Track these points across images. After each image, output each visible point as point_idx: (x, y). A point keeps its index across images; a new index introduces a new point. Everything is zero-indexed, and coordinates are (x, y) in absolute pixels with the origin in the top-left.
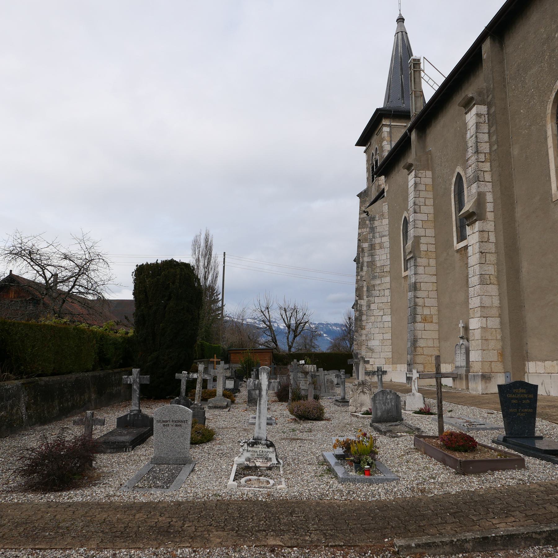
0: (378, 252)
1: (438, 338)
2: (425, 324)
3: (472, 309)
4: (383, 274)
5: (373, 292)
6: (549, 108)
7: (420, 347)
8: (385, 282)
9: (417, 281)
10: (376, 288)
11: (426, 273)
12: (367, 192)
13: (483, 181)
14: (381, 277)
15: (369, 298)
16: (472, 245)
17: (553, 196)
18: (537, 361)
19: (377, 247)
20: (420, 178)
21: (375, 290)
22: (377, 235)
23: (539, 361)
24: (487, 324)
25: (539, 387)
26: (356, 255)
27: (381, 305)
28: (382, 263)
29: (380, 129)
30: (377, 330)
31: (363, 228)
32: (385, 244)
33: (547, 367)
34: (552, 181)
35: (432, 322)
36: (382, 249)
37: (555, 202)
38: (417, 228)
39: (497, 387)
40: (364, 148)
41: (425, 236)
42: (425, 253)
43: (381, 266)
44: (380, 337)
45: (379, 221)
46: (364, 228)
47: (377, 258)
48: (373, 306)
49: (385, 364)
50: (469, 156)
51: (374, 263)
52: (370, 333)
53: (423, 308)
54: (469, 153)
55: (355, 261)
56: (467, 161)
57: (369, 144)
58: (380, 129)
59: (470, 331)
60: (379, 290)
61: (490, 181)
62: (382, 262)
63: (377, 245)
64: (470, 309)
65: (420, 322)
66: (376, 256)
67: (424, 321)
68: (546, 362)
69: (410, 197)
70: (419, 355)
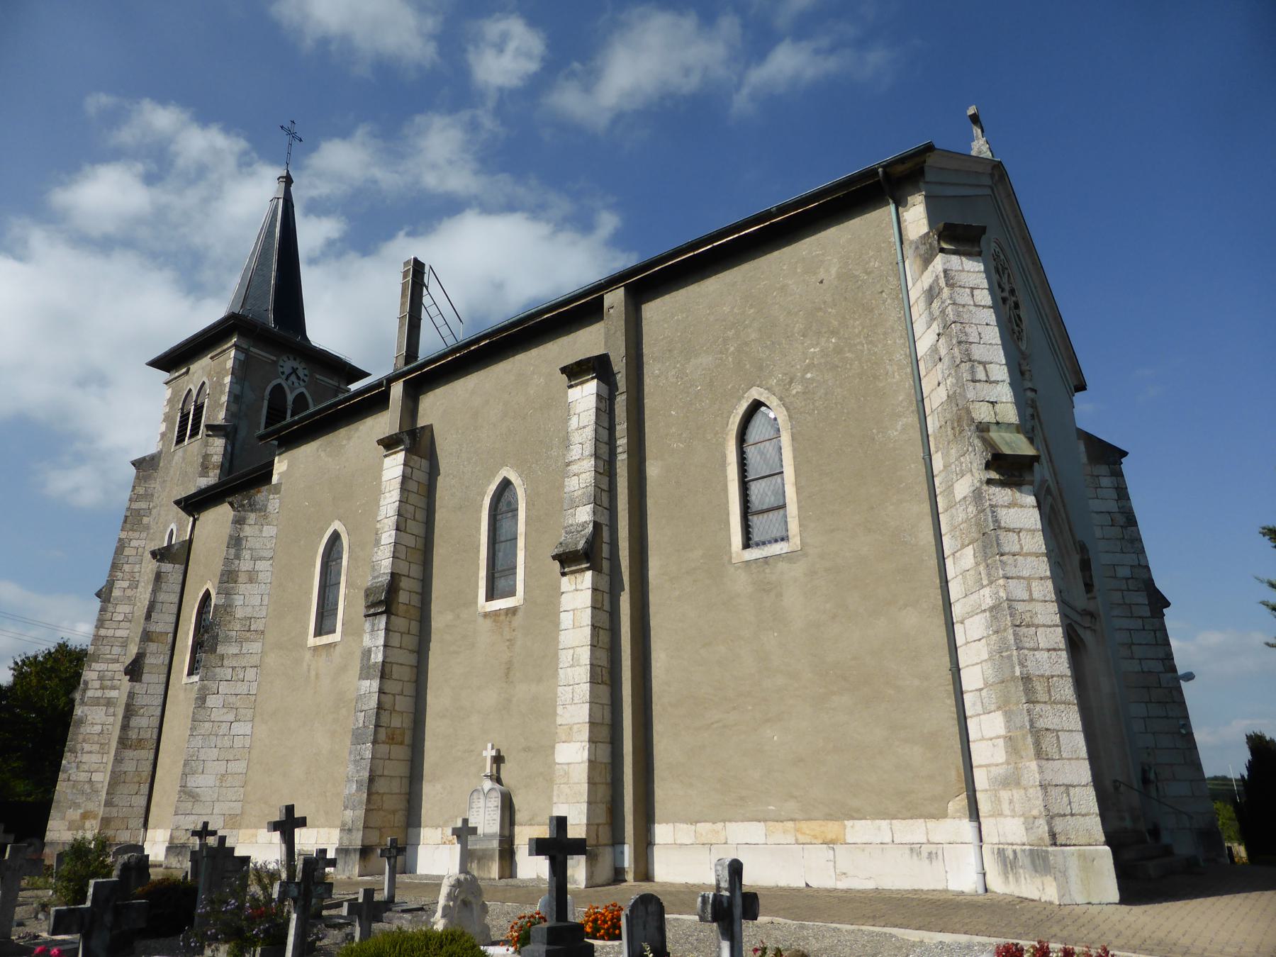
0: (243, 588)
1: (101, 755)
2: (392, 747)
3: (567, 725)
4: (248, 634)
5: (218, 670)
6: (733, 423)
7: (377, 793)
8: (250, 651)
9: (388, 660)
10: (226, 662)
11: (403, 645)
12: (156, 459)
13: (600, 506)
14: (240, 641)
15: (206, 682)
16: (574, 610)
17: (734, 555)
18: (676, 822)
19: (242, 578)
20: (412, 468)
21: (222, 666)
22: (246, 554)
23: (685, 822)
24: (595, 755)
25: (328, 852)
26: (104, 583)
27: (232, 699)
28: (248, 612)
29: (225, 351)
30: (214, 753)
31: (132, 530)
32: (261, 576)
33: (702, 835)
34: (732, 531)
35: (402, 743)
36: (254, 585)
37: (736, 565)
38: (397, 558)
39: (249, 855)
40: (165, 376)
41: (408, 576)
42: (405, 607)
43: (246, 618)
44: (220, 767)
45: (257, 527)
46: (136, 531)
47: (238, 600)
48: (212, 701)
49: (223, 828)
50: (574, 458)
51: (229, 610)
52: (195, 758)
53: (391, 713)
54: (574, 452)
55: (98, 595)
56: (568, 464)
57: (184, 370)
58: (225, 351)
59: (557, 766)
60: (233, 668)
61: (608, 508)
62: (249, 610)
63: (243, 574)
64: (560, 725)
65: (383, 743)
66: (236, 597)
67: (390, 741)
68: (698, 824)
69: (385, 498)
70: (375, 809)
